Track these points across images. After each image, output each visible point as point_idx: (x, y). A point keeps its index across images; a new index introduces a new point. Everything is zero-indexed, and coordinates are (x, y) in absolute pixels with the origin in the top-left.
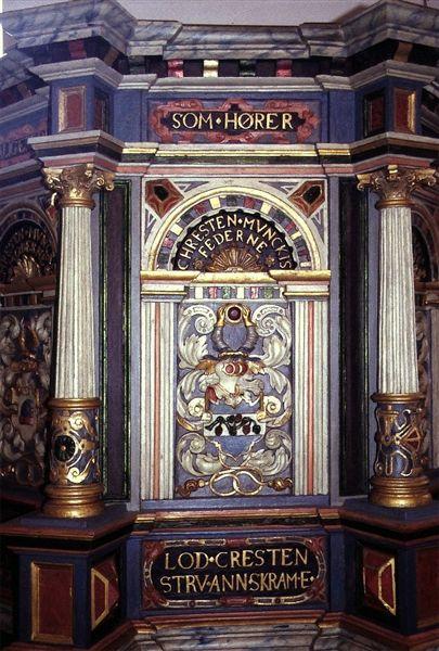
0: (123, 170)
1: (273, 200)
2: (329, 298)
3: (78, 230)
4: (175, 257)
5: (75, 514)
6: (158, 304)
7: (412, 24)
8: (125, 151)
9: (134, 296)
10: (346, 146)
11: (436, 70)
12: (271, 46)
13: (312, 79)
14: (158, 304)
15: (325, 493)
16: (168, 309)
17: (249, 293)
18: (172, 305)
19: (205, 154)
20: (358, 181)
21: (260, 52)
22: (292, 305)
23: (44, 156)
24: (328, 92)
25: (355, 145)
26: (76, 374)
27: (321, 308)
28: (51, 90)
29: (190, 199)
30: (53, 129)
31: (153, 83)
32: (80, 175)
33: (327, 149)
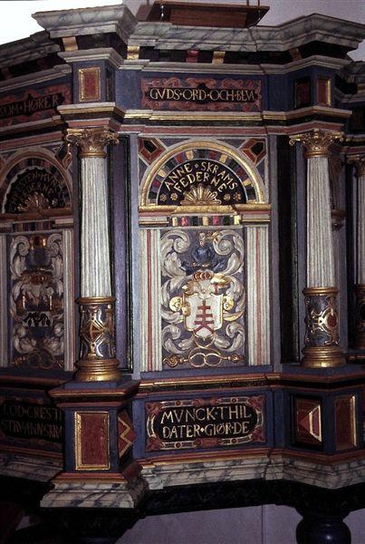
0: (124, 130)
1: (228, 152)
3: (94, 172)
4: (165, 193)
5: (324, 365)
6: (149, 231)
7: (336, 31)
8: (126, 116)
10: (282, 113)
12: (29, 52)
14: (149, 231)
17: (210, 221)
18: (159, 231)
20: (338, 139)
21: (26, 57)
22: (244, 230)
24: (268, 76)
25: (288, 113)
26: (96, 284)
27: (264, 233)
29: (169, 151)
30: (75, 99)
33: (268, 114)
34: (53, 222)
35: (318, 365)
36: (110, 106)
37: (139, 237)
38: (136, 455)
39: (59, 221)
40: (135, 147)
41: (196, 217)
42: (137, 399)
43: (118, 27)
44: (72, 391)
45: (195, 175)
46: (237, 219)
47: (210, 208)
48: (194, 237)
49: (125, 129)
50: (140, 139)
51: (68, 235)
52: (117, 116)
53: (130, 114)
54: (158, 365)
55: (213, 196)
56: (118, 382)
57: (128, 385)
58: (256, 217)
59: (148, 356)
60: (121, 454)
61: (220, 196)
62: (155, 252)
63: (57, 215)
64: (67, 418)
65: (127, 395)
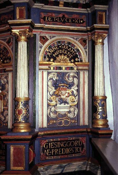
2: (88, 70)
3: (23, 46)
5: (23, 131)
9: (37, 69)
11: (46, 127)
13: (86, 9)
15: (88, 125)
16: (45, 73)
19: (101, 84)
23: (12, 26)
26: (23, 92)
28: (14, 7)
31: (42, 6)
32: (25, 32)
34: (5, 69)
35: (98, 127)
36: (30, 21)
37: (39, 74)
38: (36, 163)
39: (7, 69)
40: (38, 38)
41: (60, 67)
42: (37, 140)
43: (34, 4)
44: (9, 136)
45: (63, 51)
46: (75, 69)
47: (66, 64)
48: (59, 74)
49: (35, 32)
50: (41, 37)
51: (10, 75)
52: (32, 25)
53: (37, 25)
54: (45, 125)
55: (68, 59)
56: (30, 133)
57: (33, 134)
58: (85, 68)
59: (42, 121)
60: (30, 163)
61: (70, 60)
62: (44, 80)
63: (6, 66)
64: (8, 149)
65: (34, 136)
